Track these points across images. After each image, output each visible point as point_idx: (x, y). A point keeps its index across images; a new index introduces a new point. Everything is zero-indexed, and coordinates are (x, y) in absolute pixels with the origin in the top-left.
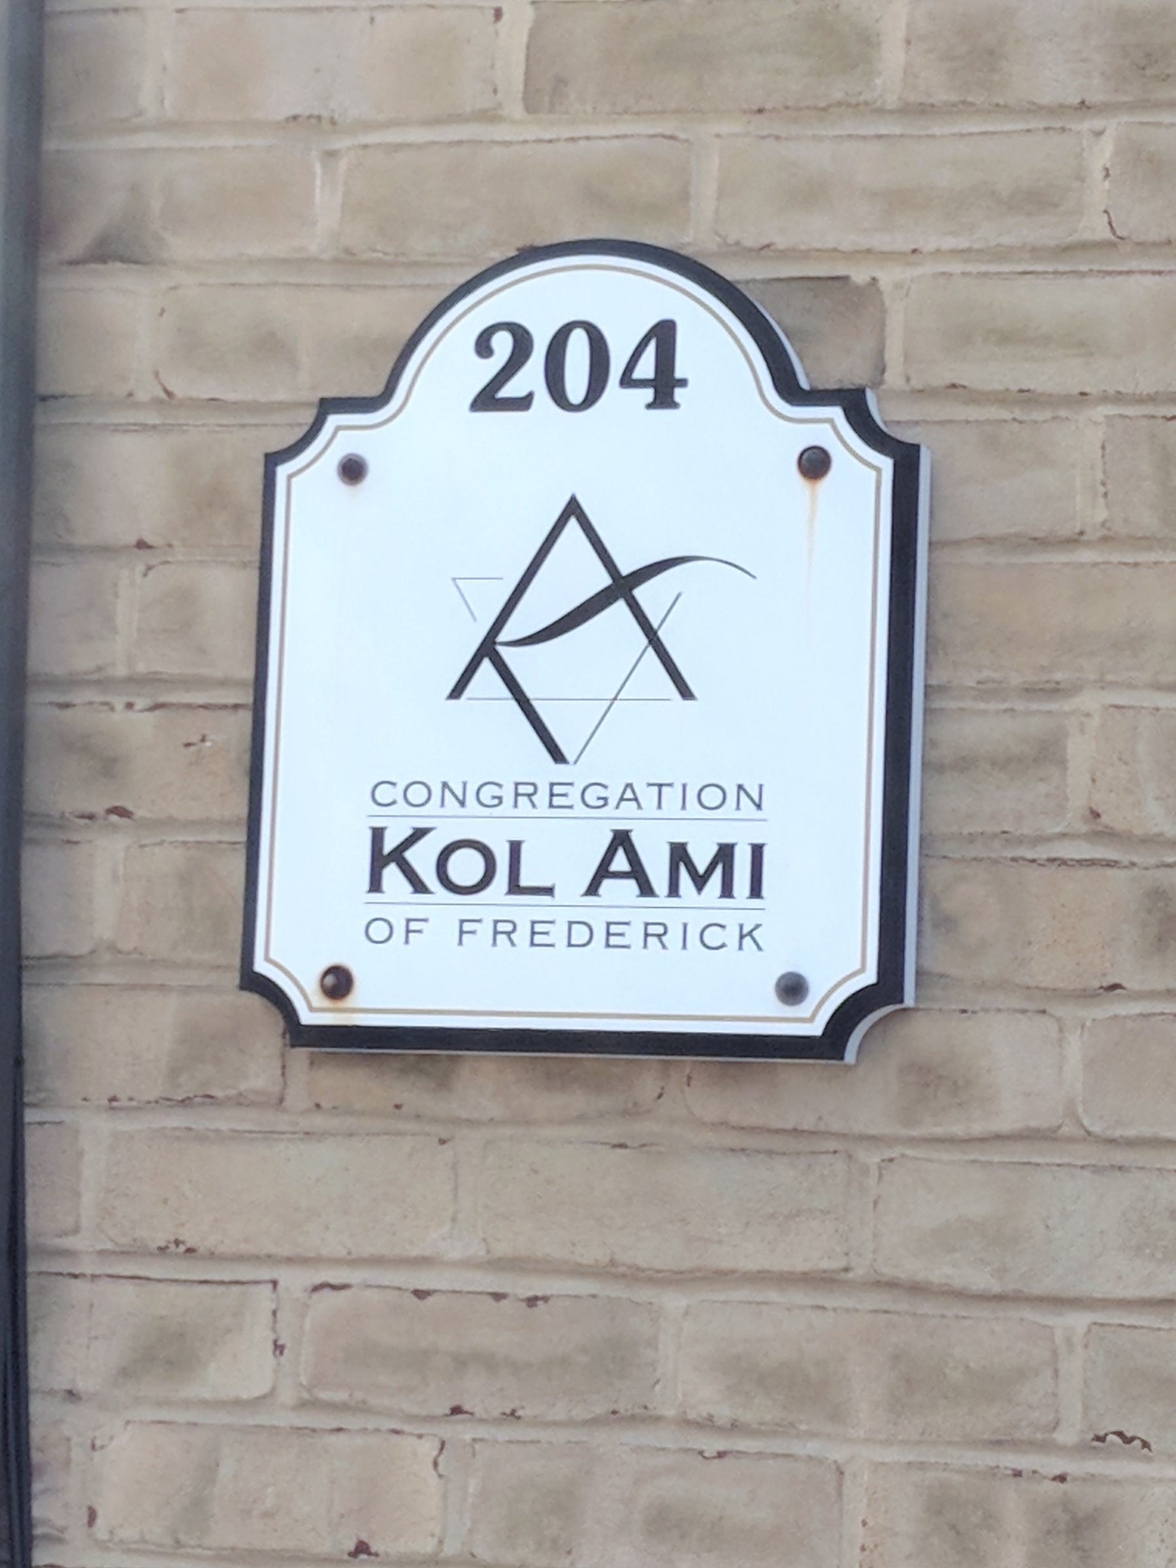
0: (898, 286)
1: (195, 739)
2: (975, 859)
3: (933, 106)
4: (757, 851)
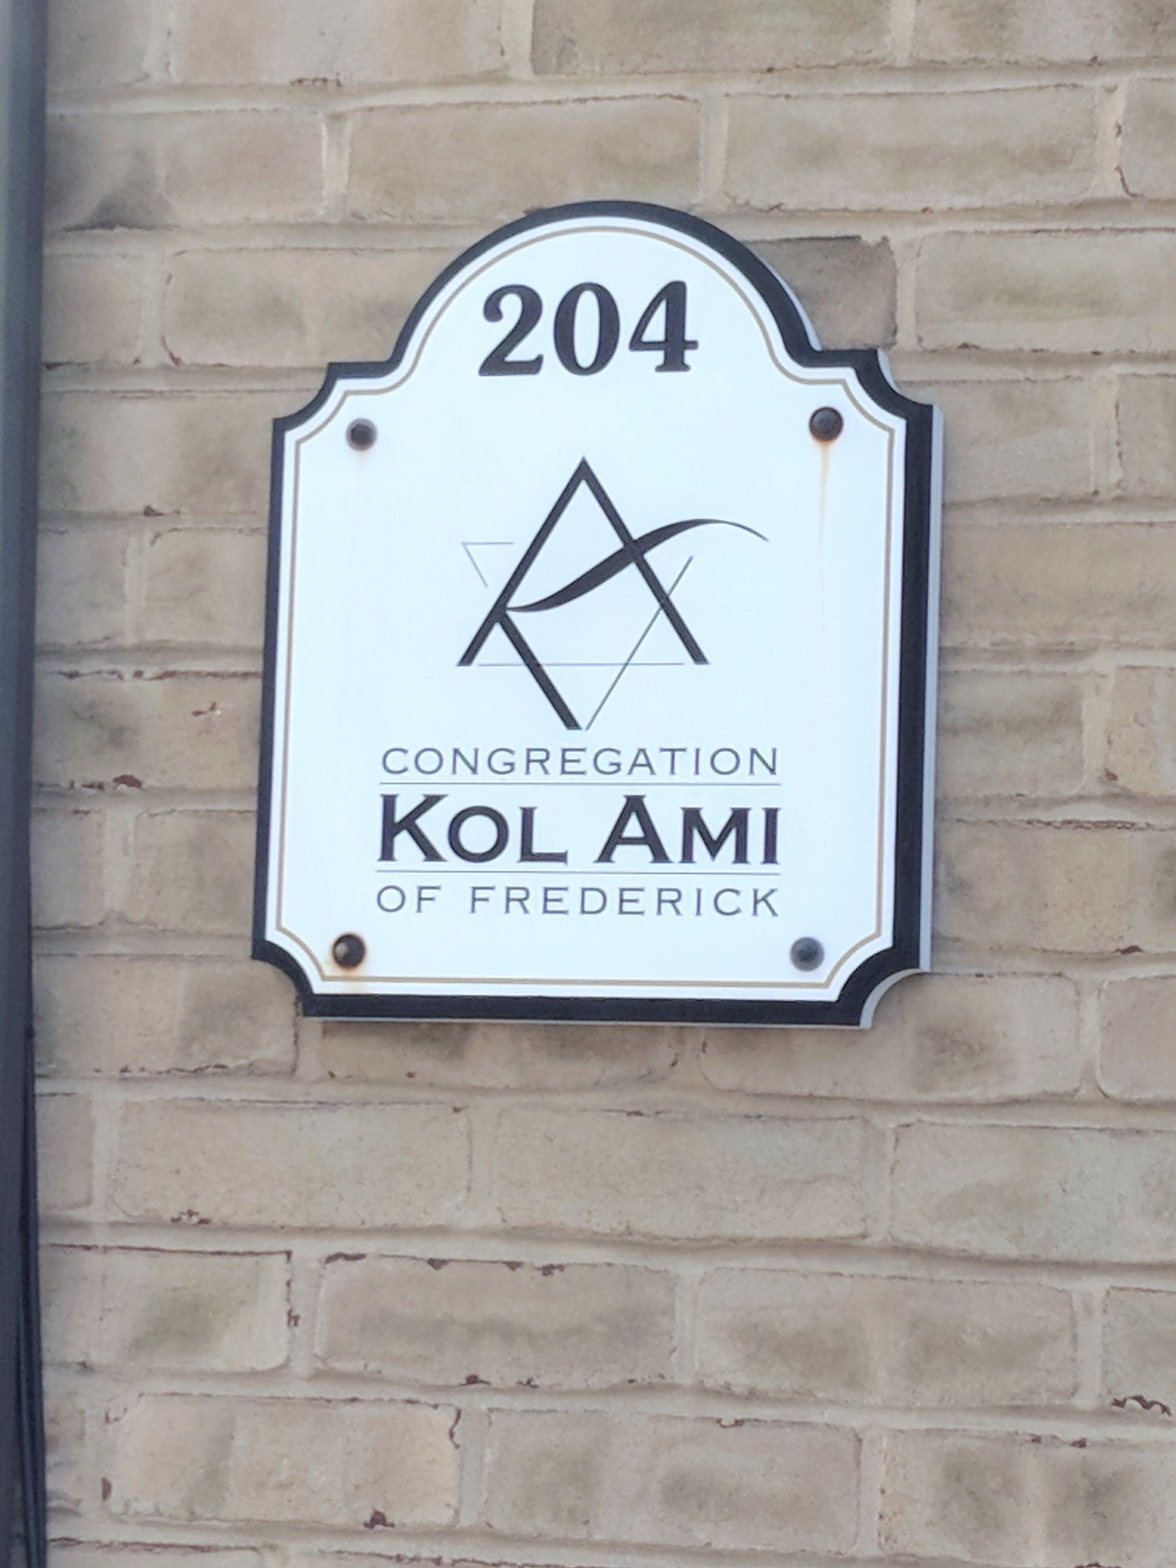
0: (910, 245)
1: (205, 707)
2: (992, 822)
3: (944, 63)
4: (771, 816)
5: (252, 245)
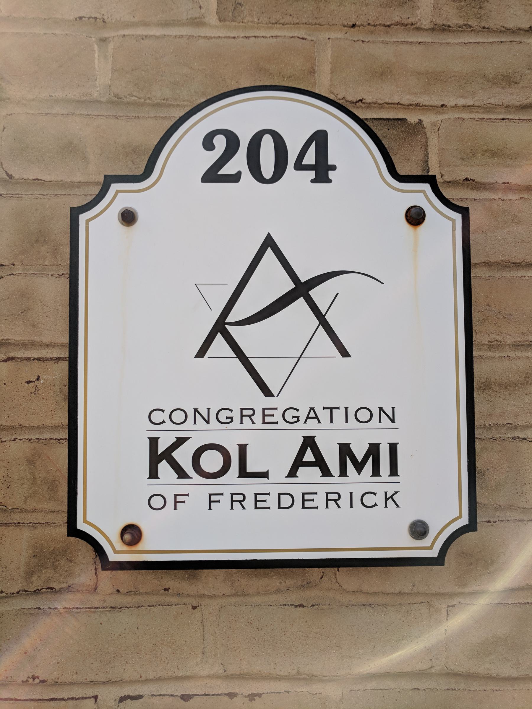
0: (434, 124)
1: (33, 379)
3: (449, 26)
4: (393, 448)
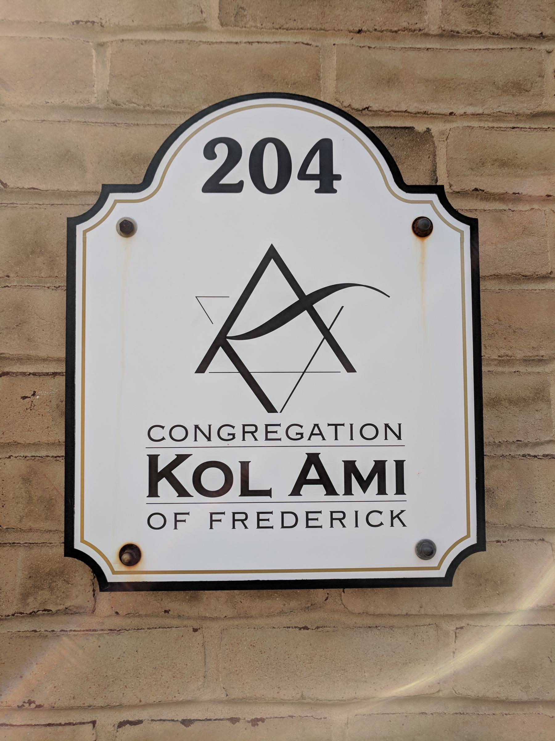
0: (442, 133)
2: (502, 456)
3: (458, 32)
4: (400, 465)
5: (50, 119)
